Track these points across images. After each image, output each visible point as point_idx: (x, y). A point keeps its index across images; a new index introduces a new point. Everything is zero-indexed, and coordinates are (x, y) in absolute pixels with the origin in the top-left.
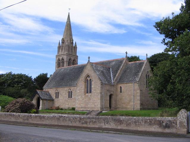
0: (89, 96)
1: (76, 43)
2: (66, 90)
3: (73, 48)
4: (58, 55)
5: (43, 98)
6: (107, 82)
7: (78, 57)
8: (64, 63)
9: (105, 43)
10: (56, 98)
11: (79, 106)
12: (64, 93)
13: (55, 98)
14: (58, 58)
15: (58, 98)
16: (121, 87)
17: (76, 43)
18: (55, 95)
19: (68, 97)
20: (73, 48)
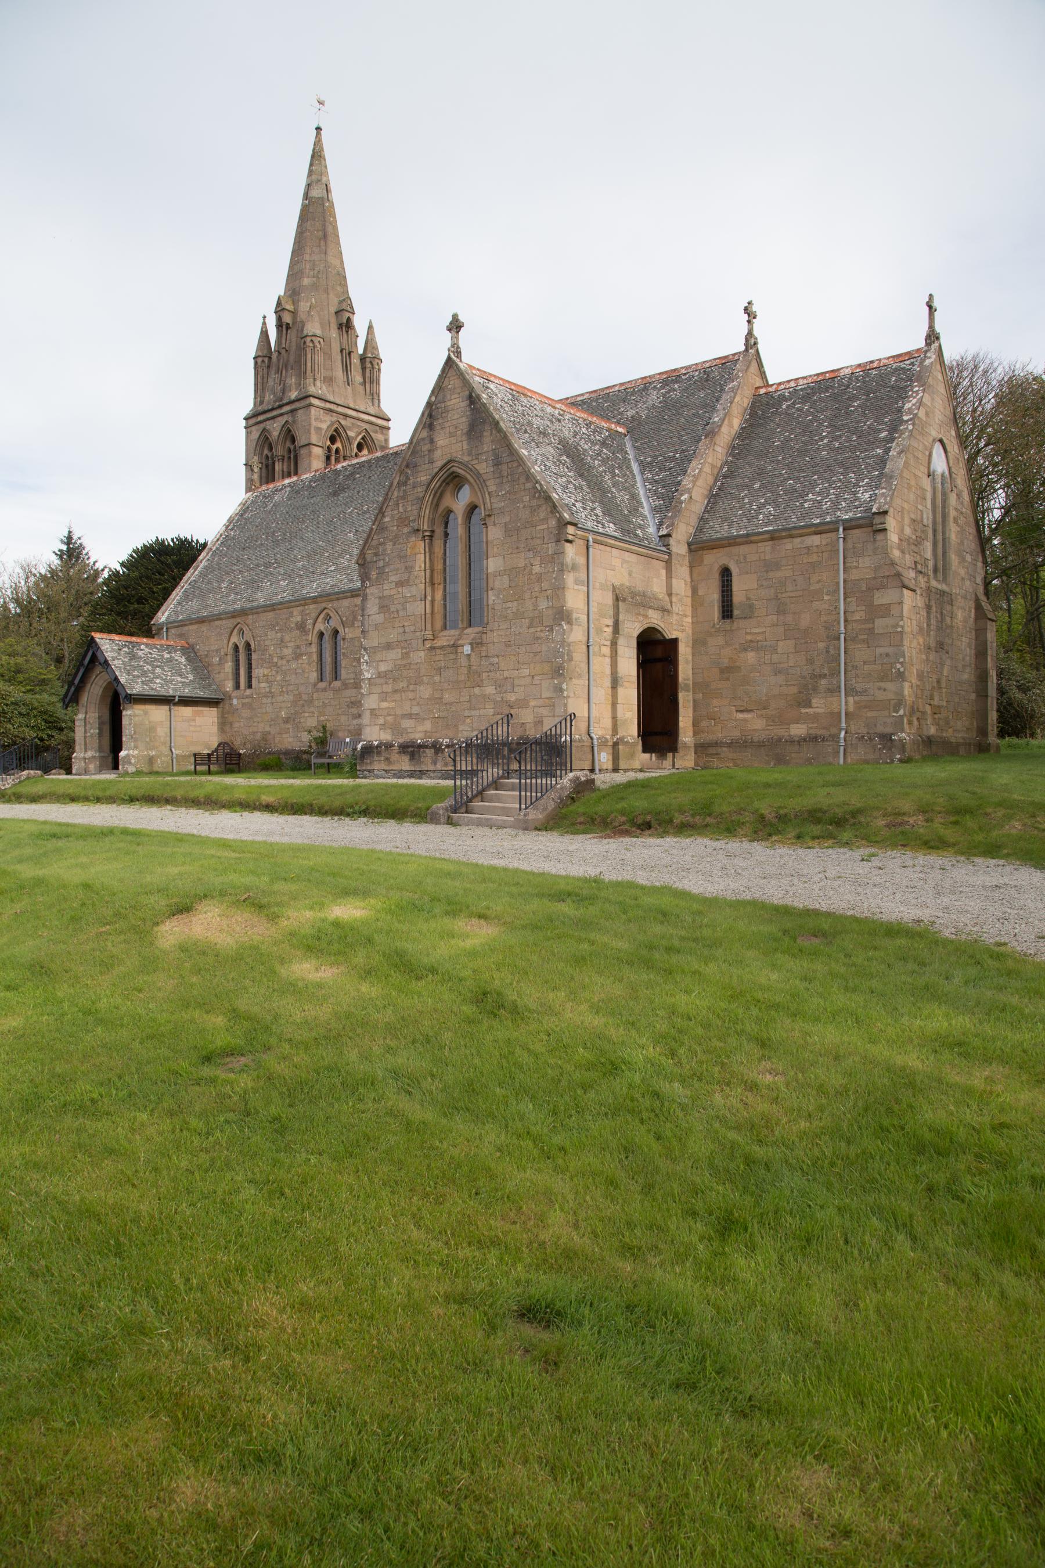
0: (467, 649)
1: (370, 328)
2: (301, 627)
3: (355, 360)
4: (260, 409)
5: (137, 688)
6: (611, 529)
7: (391, 424)
8: (296, 457)
9: (419, 823)
10: (237, 686)
11: (880, 1324)
12: (288, 652)
13: (229, 686)
14: (256, 434)
15: (250, 686)
16: (726, 574)
17: (370, 328)
18: (229, 666)
19: (314, 676)
20: (355, 360)
